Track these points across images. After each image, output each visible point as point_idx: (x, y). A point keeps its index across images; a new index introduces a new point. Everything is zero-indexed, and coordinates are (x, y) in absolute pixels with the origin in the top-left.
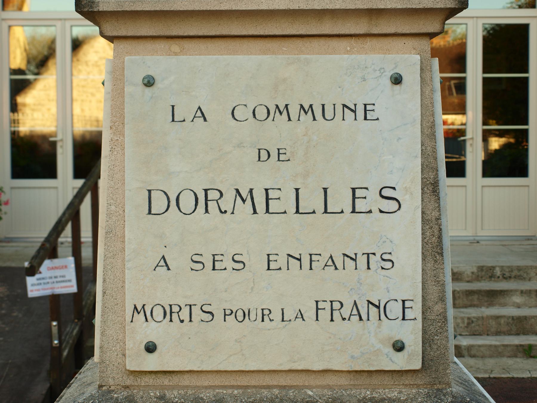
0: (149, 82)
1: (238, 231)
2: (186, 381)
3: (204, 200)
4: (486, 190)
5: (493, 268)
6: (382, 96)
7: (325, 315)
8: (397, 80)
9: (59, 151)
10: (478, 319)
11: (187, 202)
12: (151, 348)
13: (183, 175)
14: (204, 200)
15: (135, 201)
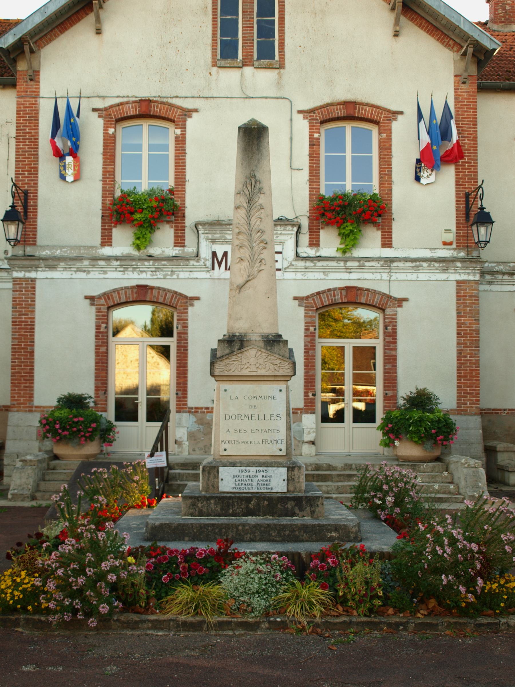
0: (225, 391)
1: (245, 424)
2: (233, 457)
3: (238, 417)
4: (355, 429)
5: (351, 465)
6: (277, 394)
7: (264, 443)
8: (281, 391)
9: (139, 407)
10: (342, 486)
11: (234, 417)
12: (225, 450)
13: (233, 411)
14: (238, 417)
15: (222, 417)
